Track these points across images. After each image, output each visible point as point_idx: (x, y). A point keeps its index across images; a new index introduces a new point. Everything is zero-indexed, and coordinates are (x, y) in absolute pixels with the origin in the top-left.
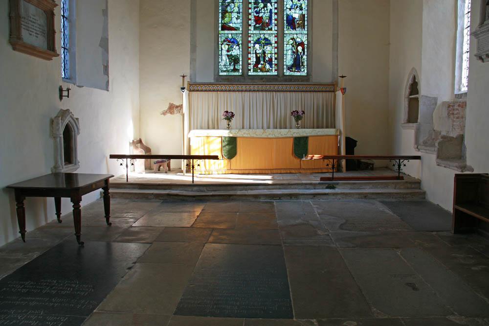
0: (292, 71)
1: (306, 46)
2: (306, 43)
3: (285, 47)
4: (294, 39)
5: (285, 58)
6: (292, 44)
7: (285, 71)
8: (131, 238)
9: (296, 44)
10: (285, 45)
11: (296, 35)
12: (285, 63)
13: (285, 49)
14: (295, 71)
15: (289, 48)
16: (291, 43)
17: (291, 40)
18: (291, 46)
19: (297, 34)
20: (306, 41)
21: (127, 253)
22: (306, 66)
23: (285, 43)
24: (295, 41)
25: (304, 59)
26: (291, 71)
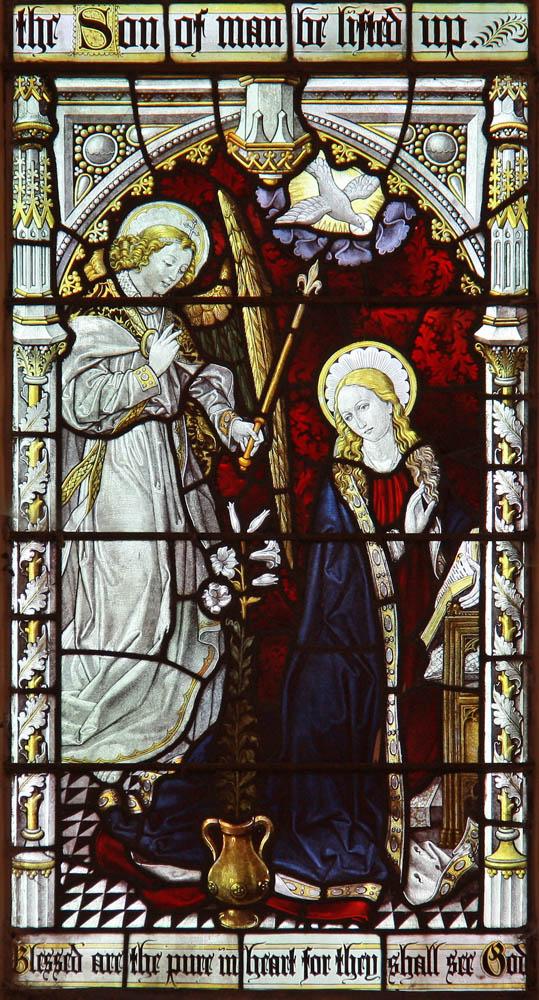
0: (202, 902)
1: (497, 330)
2: (508, 278)
3: (27, 371)
4: (243, 184)
5: (29, 600)
6: (175, 302)
7: (31, 903)
8: (315, 573)
9: (277, 299)
10: (31, 328)
11: (264, 101)
12: (26, 720)
13: (28, 415)
14: (258, 904)
15: (131, 385)
16: (168, 268)
17: (164, 219)
18: (165, 349)
19: (293, 74)
20: (510, 230)
21: (161, 239)
22: (501, 791)
23: (30, 274)
24: (259, 225)
25: (467, 626)
26: (167, 903)
